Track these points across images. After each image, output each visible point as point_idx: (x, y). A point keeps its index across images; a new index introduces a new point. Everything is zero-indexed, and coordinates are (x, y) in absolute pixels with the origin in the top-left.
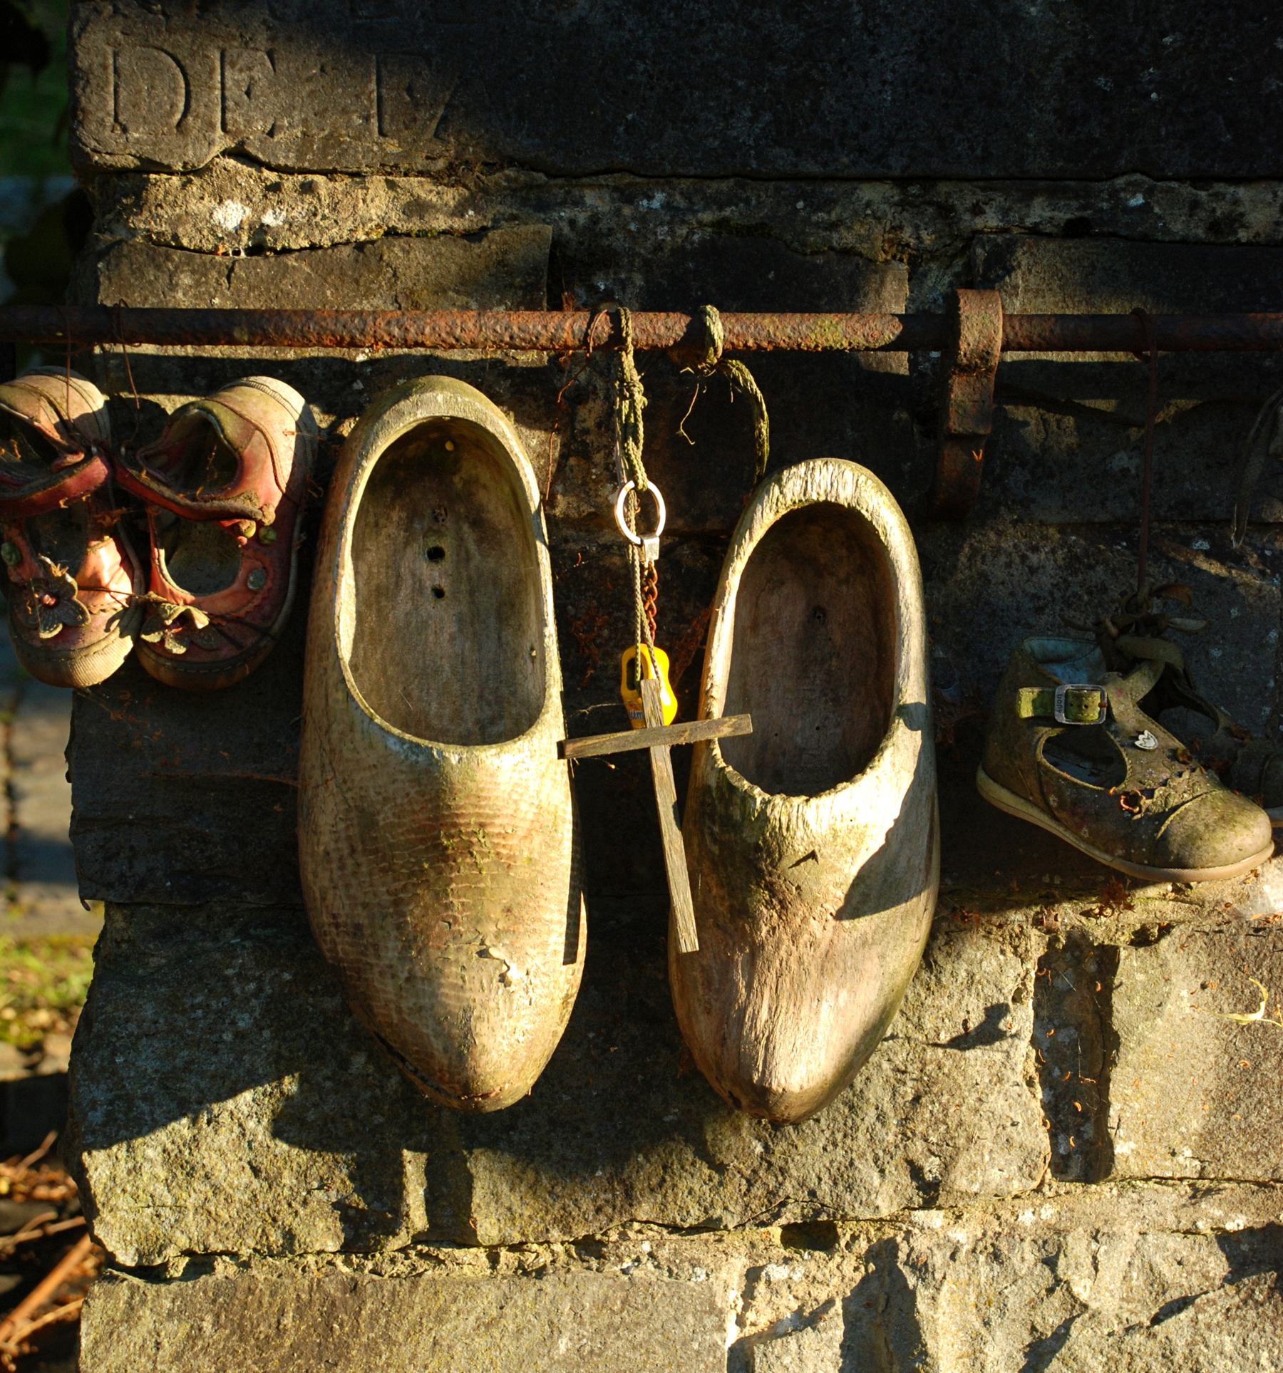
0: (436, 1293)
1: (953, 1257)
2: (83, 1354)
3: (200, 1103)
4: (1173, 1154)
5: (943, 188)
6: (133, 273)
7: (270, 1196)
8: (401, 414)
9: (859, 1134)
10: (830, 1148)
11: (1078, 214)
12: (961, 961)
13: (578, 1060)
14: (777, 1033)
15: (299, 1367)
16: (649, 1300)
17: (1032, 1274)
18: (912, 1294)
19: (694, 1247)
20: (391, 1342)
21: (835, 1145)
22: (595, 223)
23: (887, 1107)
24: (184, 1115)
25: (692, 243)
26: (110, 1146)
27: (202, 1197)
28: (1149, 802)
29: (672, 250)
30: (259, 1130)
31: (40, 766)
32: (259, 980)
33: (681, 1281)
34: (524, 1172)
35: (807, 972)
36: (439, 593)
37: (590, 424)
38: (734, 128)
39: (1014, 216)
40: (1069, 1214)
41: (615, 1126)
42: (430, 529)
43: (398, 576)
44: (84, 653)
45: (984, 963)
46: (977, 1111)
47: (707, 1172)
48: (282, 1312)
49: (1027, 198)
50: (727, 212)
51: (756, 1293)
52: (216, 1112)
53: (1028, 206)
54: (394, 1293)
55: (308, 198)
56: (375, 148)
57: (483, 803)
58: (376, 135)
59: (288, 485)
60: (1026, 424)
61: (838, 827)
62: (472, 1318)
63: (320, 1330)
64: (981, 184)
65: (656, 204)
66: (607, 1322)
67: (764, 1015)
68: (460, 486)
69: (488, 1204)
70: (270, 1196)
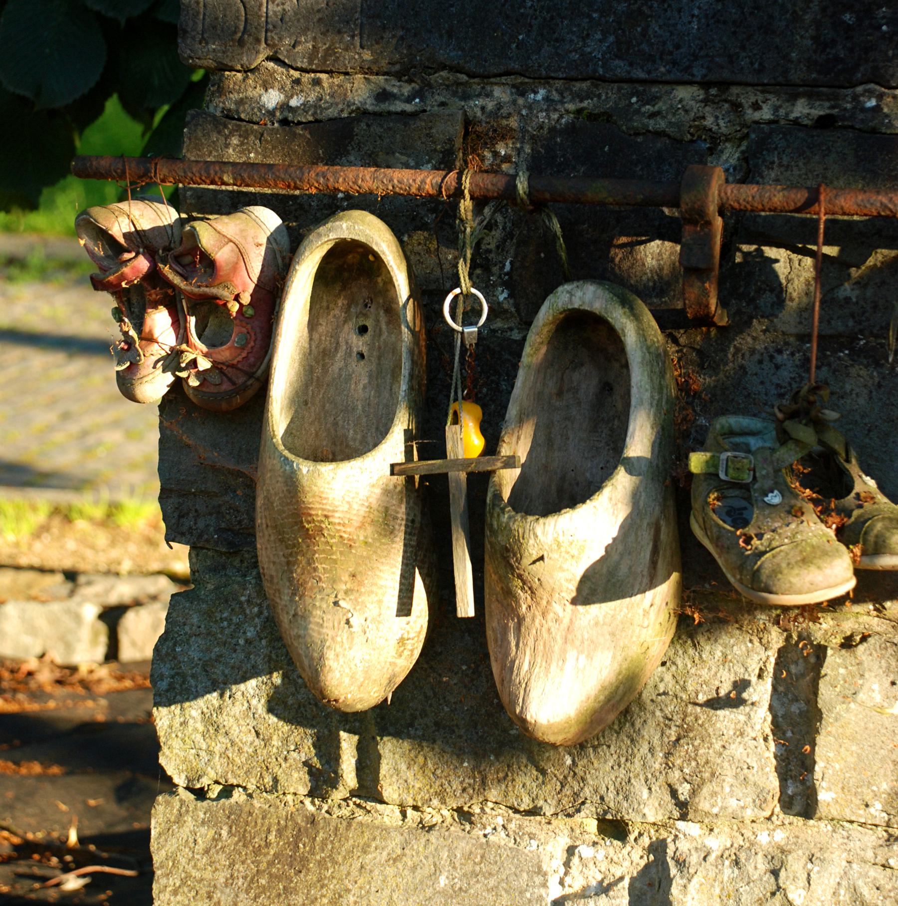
0: (362, 832)
1: (705, 859)
2: (152, 840)
3: (225, 684)
4: (867, 806)
5: (735, 90)
6: (204, 135)
7: (265, 751)
8: (319, 235)
9: (636, 760)
10: (616, 767)
11: (828, 112)
12: (717, 644)
13: (455, 684)
14: (532, 681)
15: (278, 869)
16: (498, 858)
17: (761, 880)
18: (670, 881)
19: (531, 824)
20: (335, 862)
21: (619, 766)
22: (499, 109)
23: (656, 741)
24: (215, 691)
25: (561, 124)
26: (170, 705)
27: (224, 746)
28: (758, 542)
29: (549, 128)
30: (259, 705)
31: (791, 445)
32: (260, 605)
33: (520, 848)
34: (416, 757)
35: (554, 639)
36: (361, 356)
37: (492, 246)
38: (588, 46)
39: (782, 112)
40: (795, 840)
41: (477, 733)
42: (361, 312)
43: (338, 343)
44: (139, 381)
45: (735, 648)
46: (721, 754)
47: (535, 773)
48: (269, 831)
49: (793, 98)
50: (585, 104)
51: (571, 864)
52: (234, 691)
53: (793, 105)
54: (336, 829)
55: (317, 88)
56: (357, 57)
57: (324, 501)
58: (358, 47)
59: (259, 279)
60: (777, 261)
61: (561, 539)
62: (385, 853)
63: (291, 847)
64: (760, 88)
65: (539, 97)
66: (471, 869)
67: (525, 667)
68: (381, 285)
69: (392, 776)
70: (265, 751)
